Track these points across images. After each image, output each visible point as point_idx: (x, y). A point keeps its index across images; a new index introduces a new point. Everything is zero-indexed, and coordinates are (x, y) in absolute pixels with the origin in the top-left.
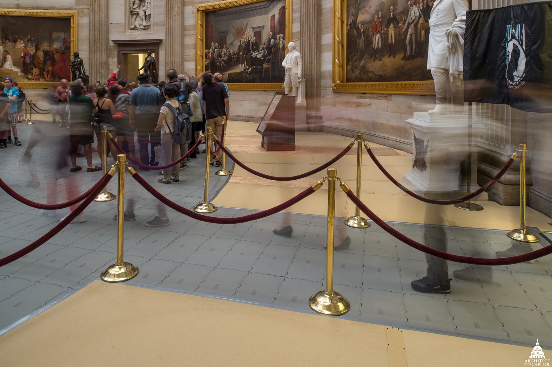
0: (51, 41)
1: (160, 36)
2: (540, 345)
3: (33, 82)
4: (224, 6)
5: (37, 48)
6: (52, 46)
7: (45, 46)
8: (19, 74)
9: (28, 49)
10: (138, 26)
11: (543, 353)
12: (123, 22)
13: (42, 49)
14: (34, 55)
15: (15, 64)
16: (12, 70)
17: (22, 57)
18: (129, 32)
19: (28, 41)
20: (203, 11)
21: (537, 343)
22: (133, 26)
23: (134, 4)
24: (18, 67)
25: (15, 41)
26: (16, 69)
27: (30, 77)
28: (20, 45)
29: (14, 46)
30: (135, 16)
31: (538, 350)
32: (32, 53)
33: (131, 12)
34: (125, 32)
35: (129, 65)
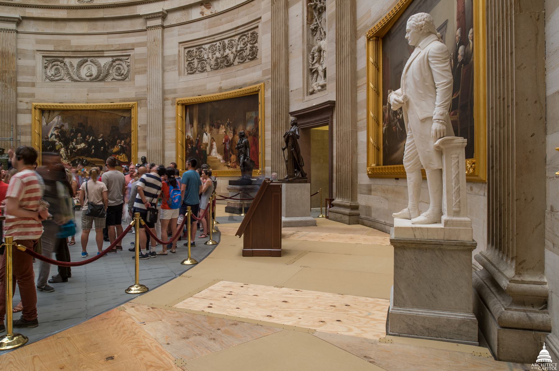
0: (245, 123)
1: (330, 95)
2: (546, 349)
3: (231, 169)
4: (207, 99)
5: (234, 133)
6: (246, 129)
7: (240, 130)
8: (222, 161)
9: (228, 134)
10: (316, 89)
11: (550, 357)
12: (301, 86)
13: (238, 133)
14: (232, 140)
15: (219, 151)
16: (217, 158)
17: (223, 143)
18: (307, 98)
19: (227, 126)
20: (183, 105)
21: (544, 347)
22: (311, 90)
23: (313, 58)
24: (221, 154)
25: (218, 127)
26: (220, 157)
27: (229, 164)
28: (222, 130)
29: (218, 132)
30: (315, 75)
31: (544, 354)
32: (230, 138)
33: (311, 70)
34: (303, 99)
35: (313, 145)
